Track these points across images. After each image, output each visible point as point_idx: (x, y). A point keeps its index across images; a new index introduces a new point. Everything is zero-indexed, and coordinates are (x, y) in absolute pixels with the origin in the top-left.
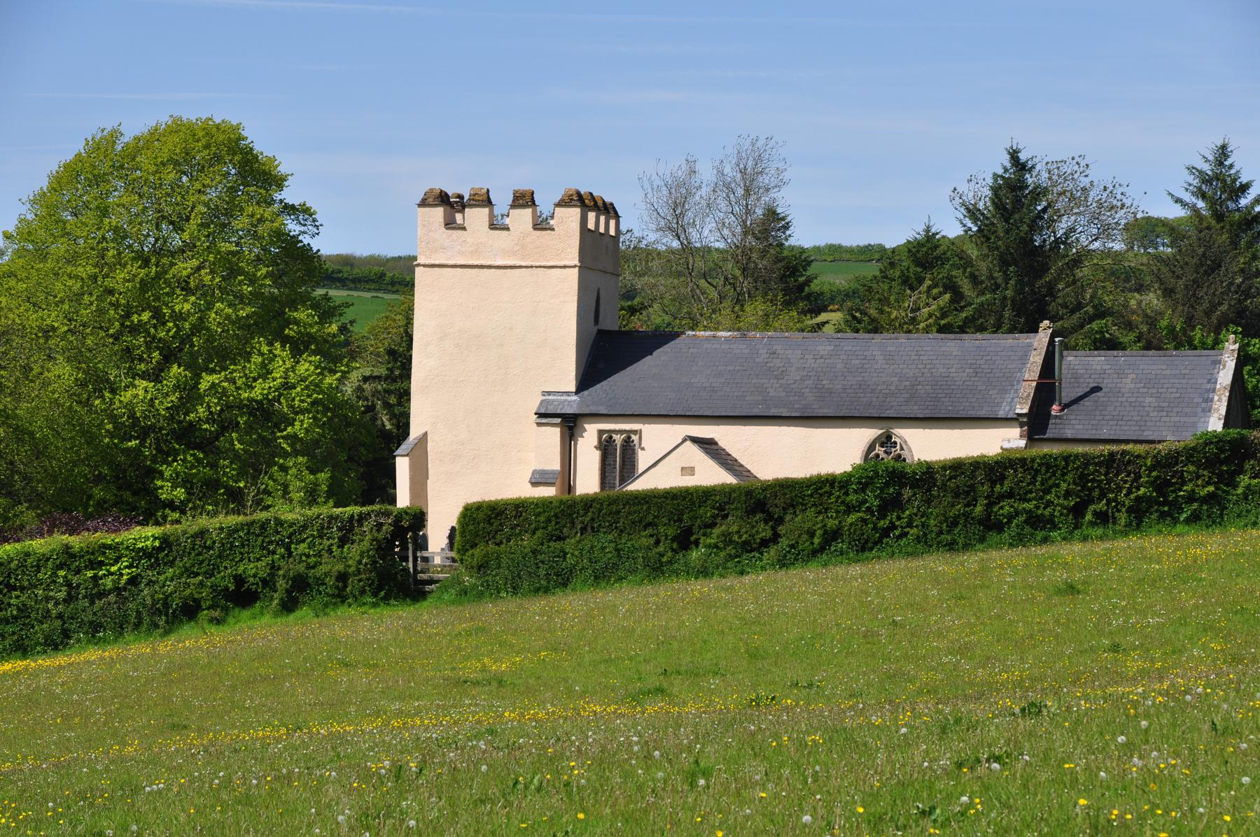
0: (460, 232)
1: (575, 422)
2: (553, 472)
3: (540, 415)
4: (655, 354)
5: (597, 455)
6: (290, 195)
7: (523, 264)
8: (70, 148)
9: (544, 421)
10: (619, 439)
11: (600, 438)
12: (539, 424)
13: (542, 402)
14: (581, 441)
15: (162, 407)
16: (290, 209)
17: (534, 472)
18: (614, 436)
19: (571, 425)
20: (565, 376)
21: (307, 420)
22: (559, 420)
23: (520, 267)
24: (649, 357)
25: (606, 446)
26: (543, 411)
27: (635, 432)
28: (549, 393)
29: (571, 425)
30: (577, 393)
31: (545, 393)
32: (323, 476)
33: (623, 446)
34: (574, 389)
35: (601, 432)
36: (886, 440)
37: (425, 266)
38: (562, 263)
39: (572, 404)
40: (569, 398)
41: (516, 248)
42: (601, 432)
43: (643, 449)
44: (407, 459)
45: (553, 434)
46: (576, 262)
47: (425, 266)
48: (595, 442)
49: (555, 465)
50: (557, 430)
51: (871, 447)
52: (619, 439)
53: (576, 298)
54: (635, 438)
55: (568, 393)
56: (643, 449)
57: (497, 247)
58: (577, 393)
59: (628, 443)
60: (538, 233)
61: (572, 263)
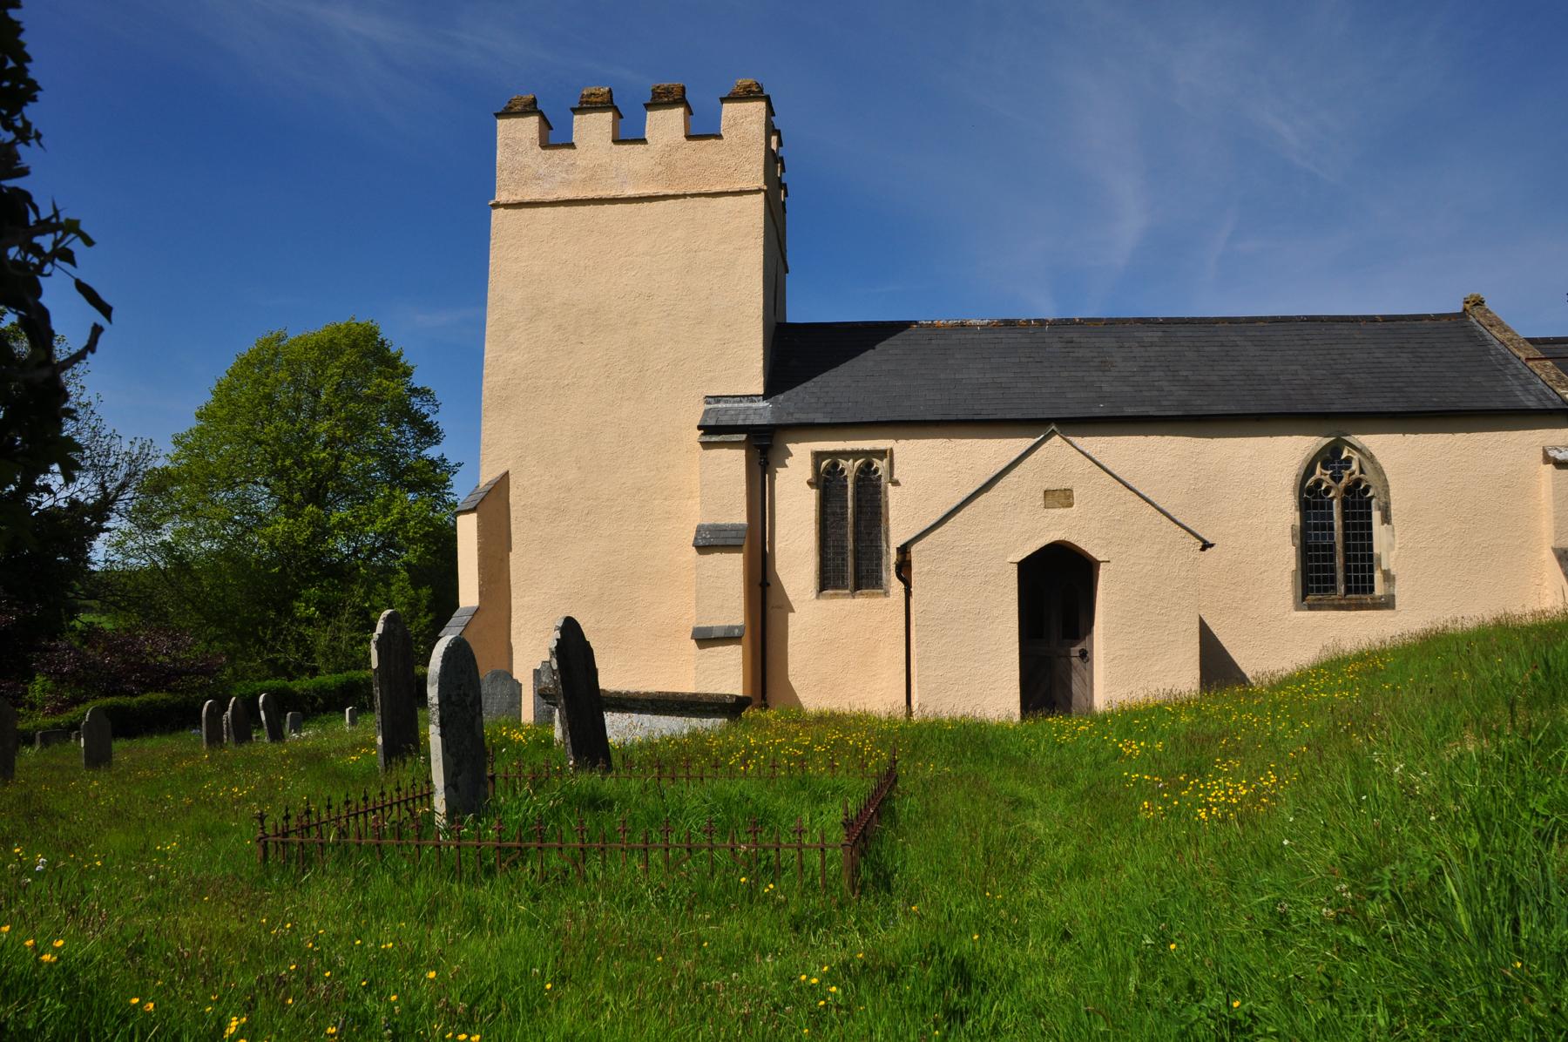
0: (566, 151)
1: (771, 438)
2: (735, 528)
3: (706, 429)
4: (879, 347)
5: (812, 496)
6: (417, 381)
7: (671, 192)
8: (247, 345)
9: (715, 439)
10: (850, 467)
11: (816, 466)
12: (706, 445)
13: (706, 412)
14: (781, 474)
15: (300, 539)
16: (414, 392)
17: (700, 529)
18: (842, 463)
19: (764, 448)
20: (745, 373)
21: (420, 549)
22: (743, 437)
23: (665, 197)
24: (871, 352)
25: (826, 480)
26: (712, 422)
27: (881, 454)
28: (718, 399)
29: (764, 448)
30: (766, 397)
31: (710, 399)
32: (425, 591)
33: (857, 480)
34: (761, 391)
35: (818, 456)
36: (1331, 457)
37: (507, 206)
38: (737, 188)
39: (762, 412)
40: (754, 405)
41: (659, 169)
42: (818, 456)
43: (896, 483)
44: (473, 517)
45: (733, 462)
46: (760, 184)
47: (507, 206)
48: (809, 474)
49: (738, 516)
50: (740, 454)
51: (1309, 470)
52: (850, 467)
53: (761, 241)
54: (880, 465)
55: (750, 398)
56: (896, 483)
57: (631, 168)
58: (766, 397)
59: (866, 473)
60: (693, 143)
61: (754, 187)
